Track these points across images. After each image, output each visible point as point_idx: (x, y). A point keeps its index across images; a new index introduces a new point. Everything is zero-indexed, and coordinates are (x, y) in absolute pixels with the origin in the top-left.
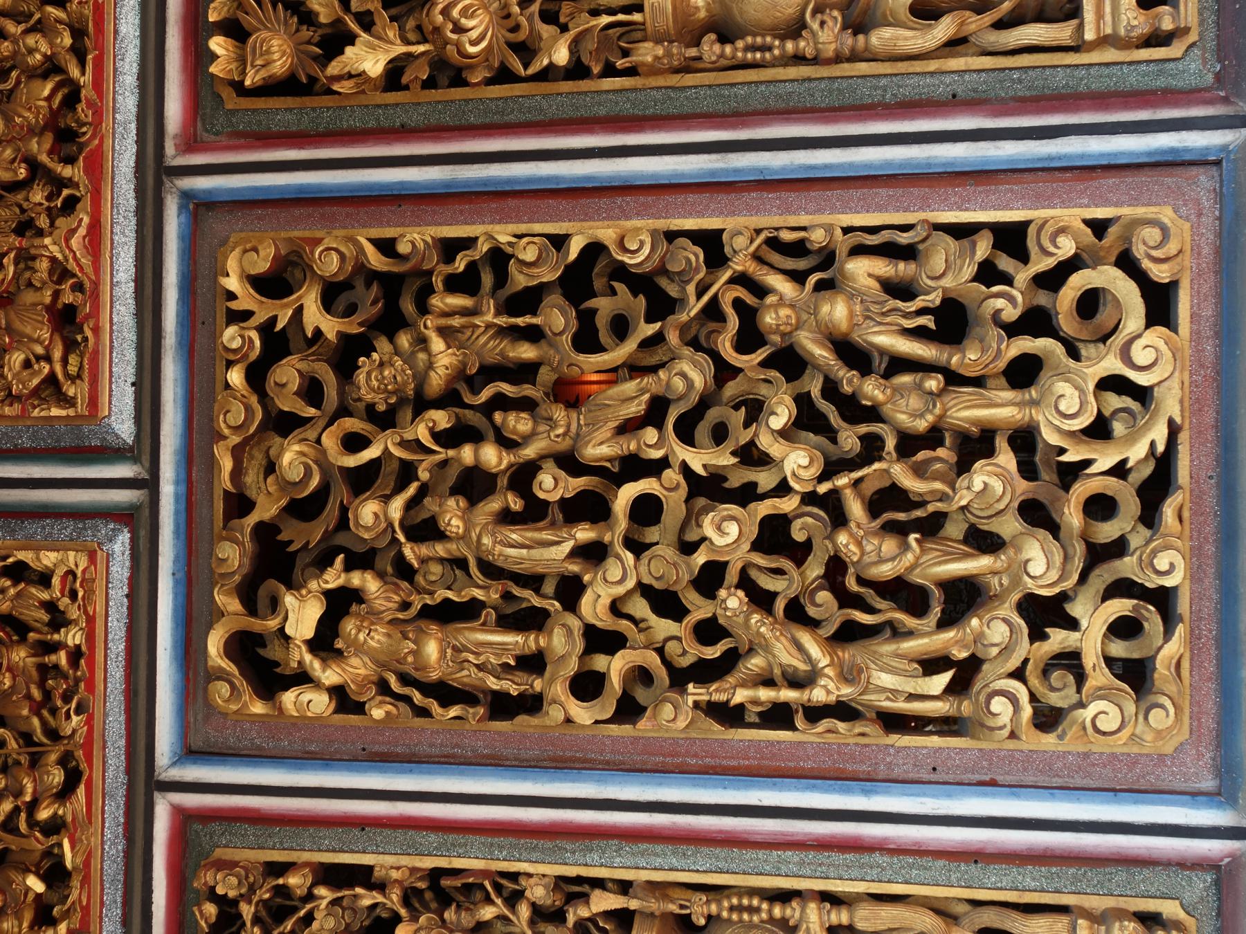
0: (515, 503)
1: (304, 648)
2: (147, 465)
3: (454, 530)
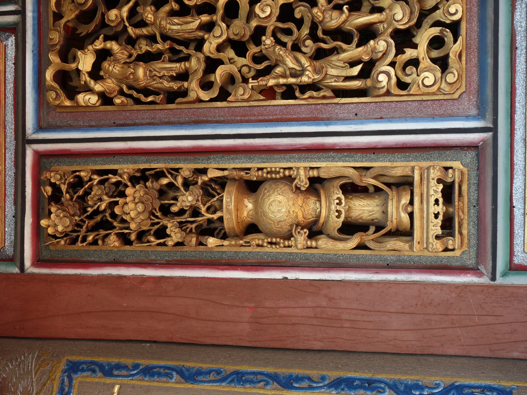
0: (175, 6)
1: (86, 75)
2: (20, 4)
3: (150, 19)
